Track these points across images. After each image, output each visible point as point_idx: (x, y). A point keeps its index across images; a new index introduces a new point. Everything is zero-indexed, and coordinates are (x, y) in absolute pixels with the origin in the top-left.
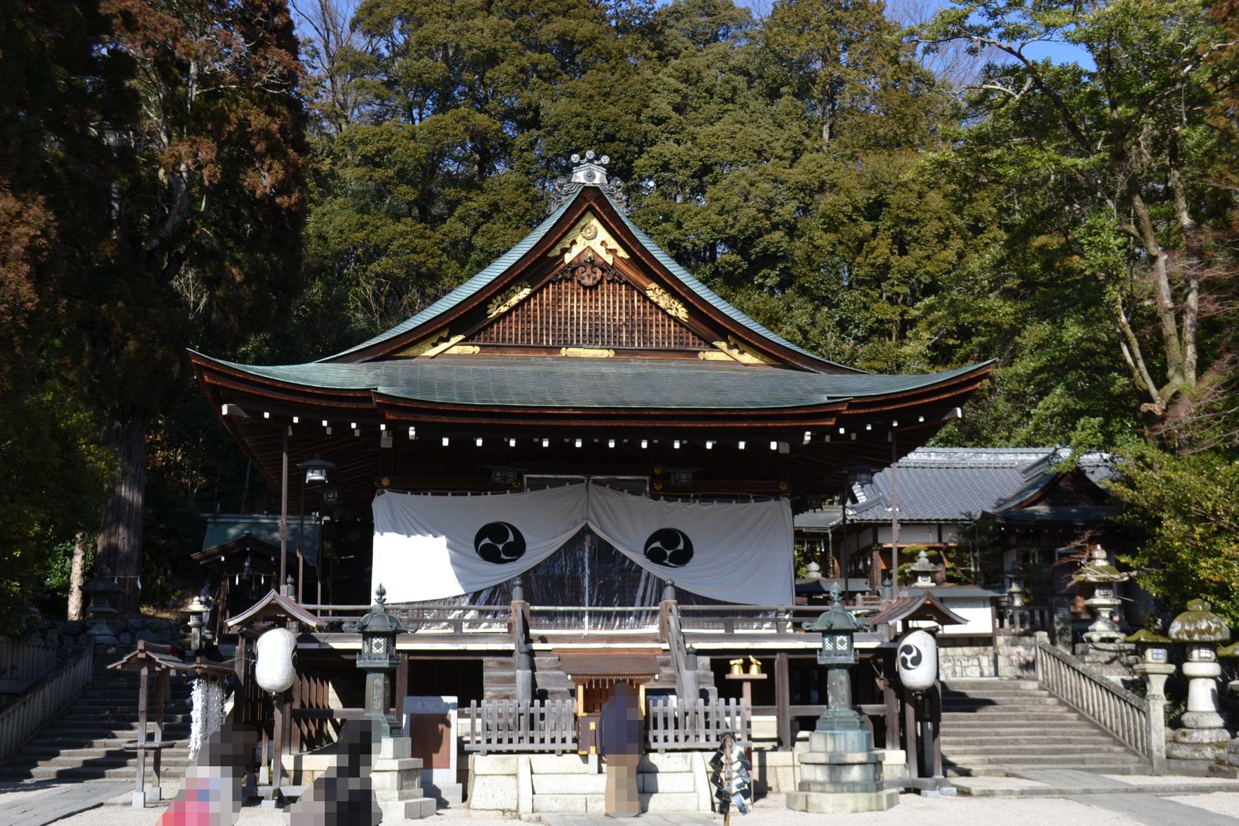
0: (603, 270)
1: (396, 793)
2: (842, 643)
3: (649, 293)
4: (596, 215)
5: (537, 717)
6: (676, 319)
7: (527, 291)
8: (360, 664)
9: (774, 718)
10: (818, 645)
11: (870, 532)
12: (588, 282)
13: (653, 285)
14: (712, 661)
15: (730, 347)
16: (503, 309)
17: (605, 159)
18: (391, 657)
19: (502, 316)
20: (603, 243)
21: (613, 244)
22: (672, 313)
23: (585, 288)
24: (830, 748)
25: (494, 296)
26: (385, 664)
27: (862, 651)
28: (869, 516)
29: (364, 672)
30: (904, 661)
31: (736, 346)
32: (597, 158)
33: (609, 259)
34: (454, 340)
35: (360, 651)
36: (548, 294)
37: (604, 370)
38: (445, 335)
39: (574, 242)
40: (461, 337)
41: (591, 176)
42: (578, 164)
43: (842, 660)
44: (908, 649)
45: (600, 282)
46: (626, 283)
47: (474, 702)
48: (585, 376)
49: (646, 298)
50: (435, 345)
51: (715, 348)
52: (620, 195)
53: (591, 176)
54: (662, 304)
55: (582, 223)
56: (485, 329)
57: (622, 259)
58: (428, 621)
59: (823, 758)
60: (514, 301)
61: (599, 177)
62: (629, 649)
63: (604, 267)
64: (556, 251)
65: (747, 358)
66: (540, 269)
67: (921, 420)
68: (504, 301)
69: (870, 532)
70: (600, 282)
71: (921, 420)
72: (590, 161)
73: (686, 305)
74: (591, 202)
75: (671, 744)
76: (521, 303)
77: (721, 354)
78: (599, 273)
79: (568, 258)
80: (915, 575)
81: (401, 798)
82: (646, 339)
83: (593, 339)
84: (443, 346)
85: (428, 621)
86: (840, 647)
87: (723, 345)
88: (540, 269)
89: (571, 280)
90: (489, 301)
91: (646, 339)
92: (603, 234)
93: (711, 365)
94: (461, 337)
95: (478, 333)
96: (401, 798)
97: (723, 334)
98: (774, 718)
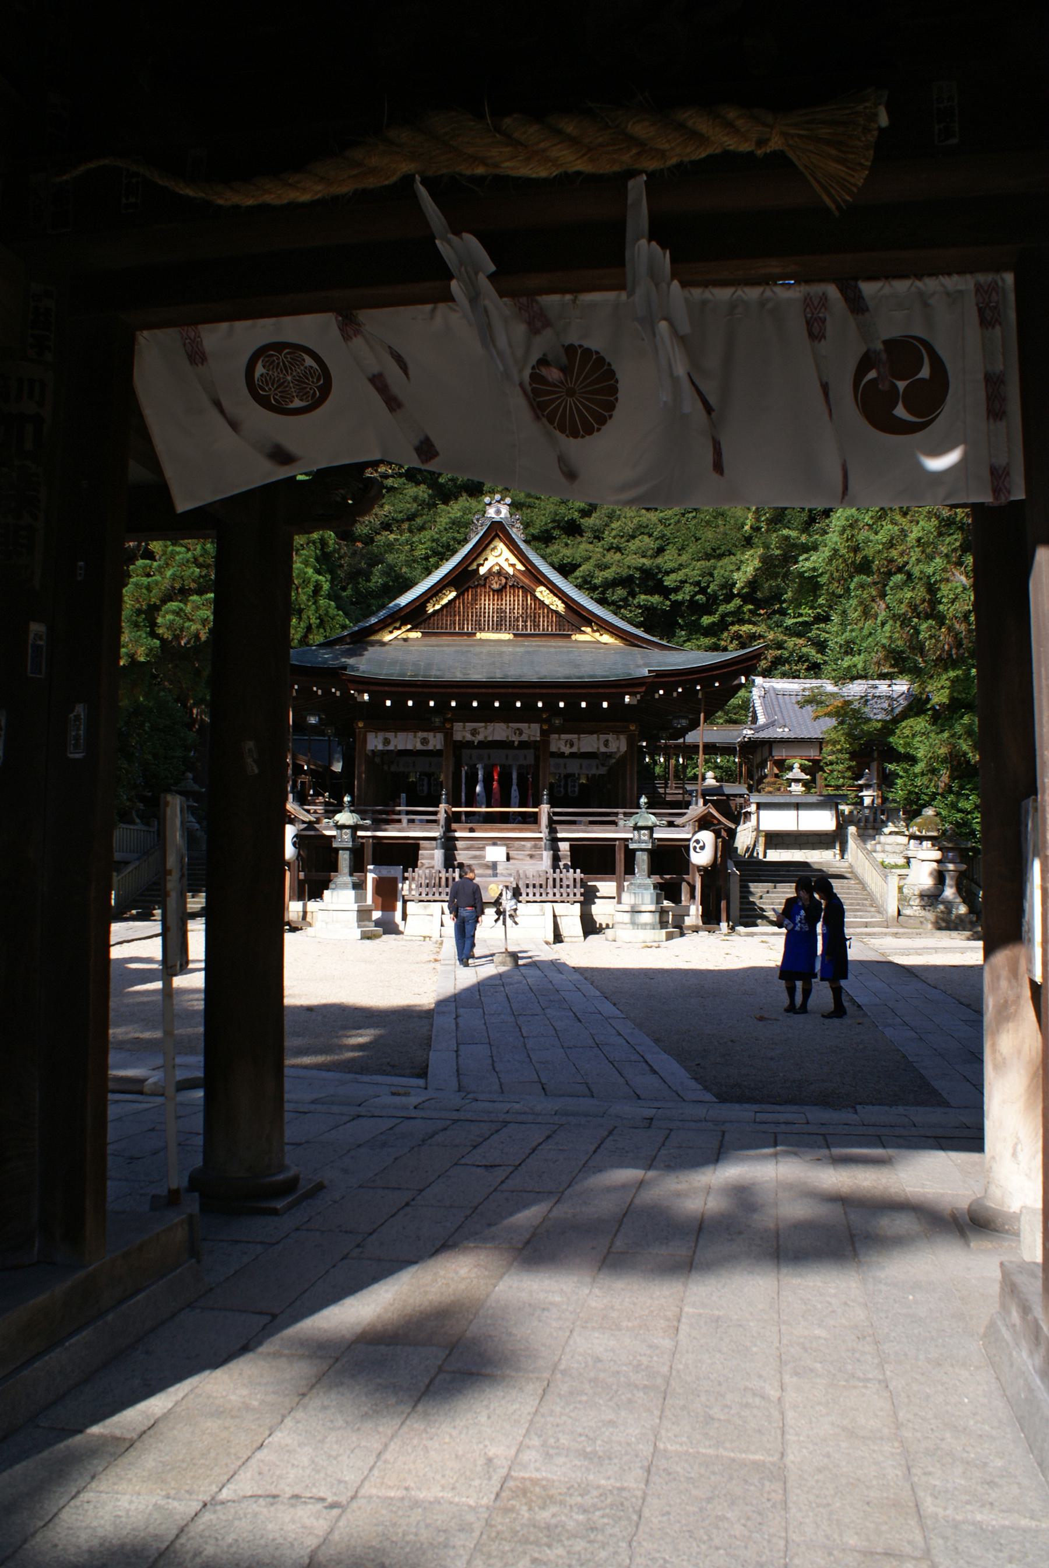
0: (506, 578)
1: (356, 924)
2: (644, 835)
3: (538, 594)
4: (501, 540)
5: (558, 881)
6: (556, 612)
7: (454, 594)
8: (334, 845)
9: (615, 884)
10: (630, 836)
11: (767, 747)
12: (495, 586)
13: (542, 588)
14: (571, 845)
15: (594, 631)
16: (438, 607)
17: (508, 500)
18: (353, 841)
19: (436, 612)
20: (507, 560)
21: (513, 560)
22: (553, 607)
23: (494, 591)
24: (633, 902)
25: (431, 598)
26: (350, 845)
27: (660, 840)
28: (763, 735)
29: (337, 850)
30: (695, 848)
31: (598, 631)
32: (502, 499)
33: (511, 571)
34: (404, 629)
35: (334, 837)
36: (469, 596)
37: (505, 649)
38: (397, 625)
39: (486, 559)
40: (409, 626)
41: (498, 512)
42: (490, 504)
43: (643, 846)
44: (697, 842)
45: (505, 587)
46: (522, 587)
47: (410, 869)
48: (489, 654)
49: (535, 598)
50: (391, 632)
51: (584, 632)
52: (518, 525)
53: (498, 512)
54: (547, 602)
55: (492, 546)
56: (425, 620)
57: (519, 570)
58: (905, 715)
59: (628, 909)
60: (445, 601)
61: (505, 511)
62: (578, 831)
63: (507, 577)
64: (474, 566)
65: (606, 638)
66: (464, 579)
67: (717, 684)
68: (438, 602)
69: (767, 747)
70: (505, 587)
71: (717, 684)
72: (499, 502)
73: (563, 602)
74: (497, 531)
75: (531, 898)
76: (450, 602)
77: (587, 636)
78: (504, 581)
79: (482, 571)
80: (790, 782)
81: (359, 927)
82: (536, 625)
83: (498, 627)
84: (396, 633)
85: (905, 715)
86: (643, 837)
87: (589, 630)
88: (464, 579)
89: (484, 586)
90: (427, 601)
91: (536, 625)
92: (507, 553)
93: (580, 645)
94: (409, 626)
95: (421, 623)
96: (359, 927)
97: (589, 623)
98: (615, 884)
